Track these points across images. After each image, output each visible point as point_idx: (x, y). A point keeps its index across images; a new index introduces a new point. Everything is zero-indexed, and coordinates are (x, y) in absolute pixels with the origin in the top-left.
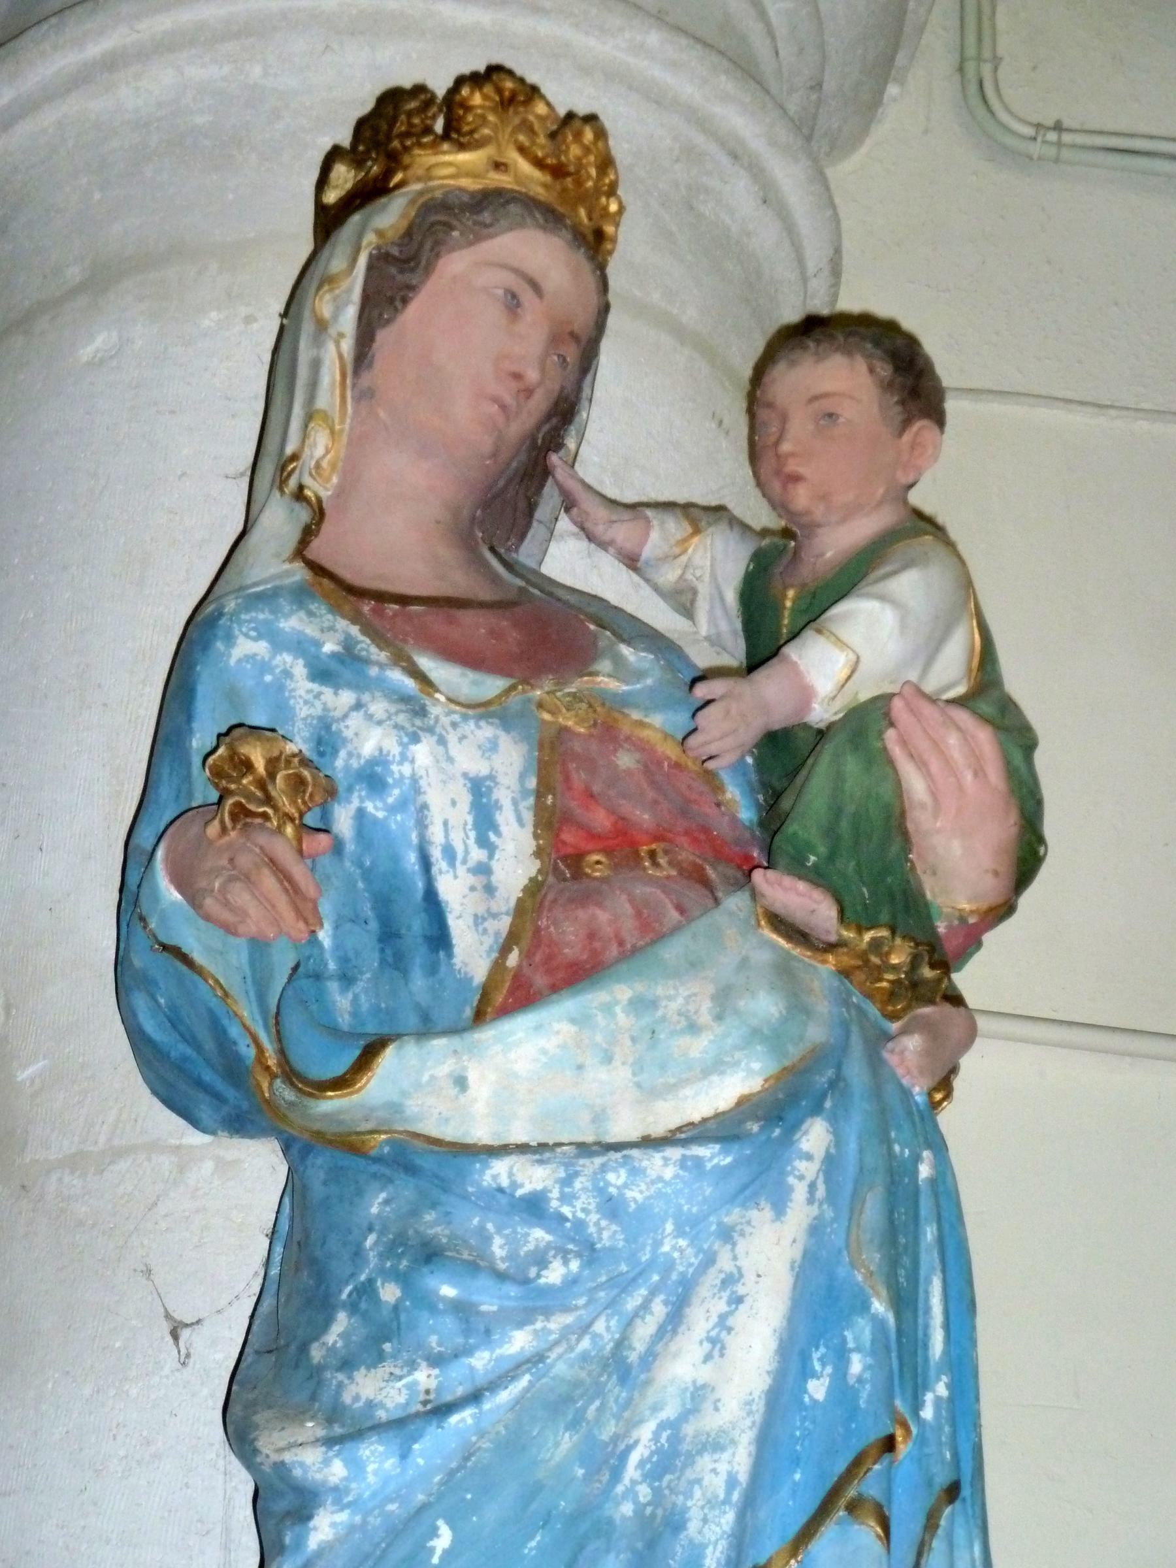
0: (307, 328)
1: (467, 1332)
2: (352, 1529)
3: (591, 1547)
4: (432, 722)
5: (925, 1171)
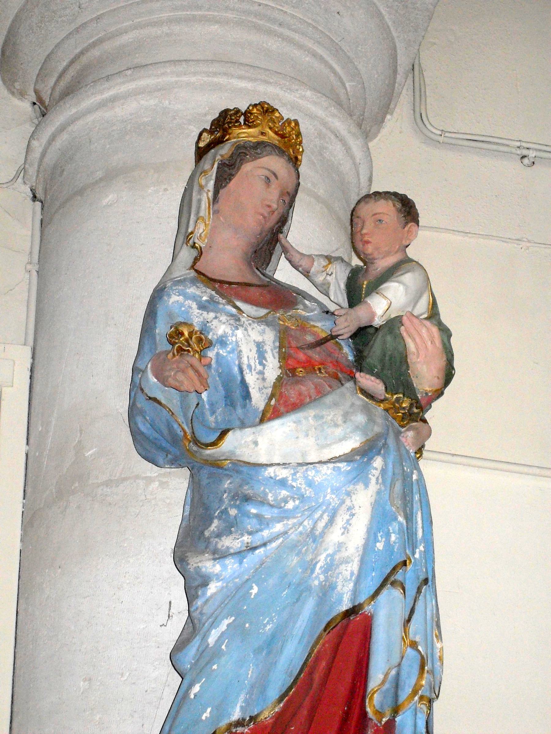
0: (196, 188)
1: (260, 524)
2: (222, 588)
3: (304, 594)
4: (242, 323)
5: (415, 477)
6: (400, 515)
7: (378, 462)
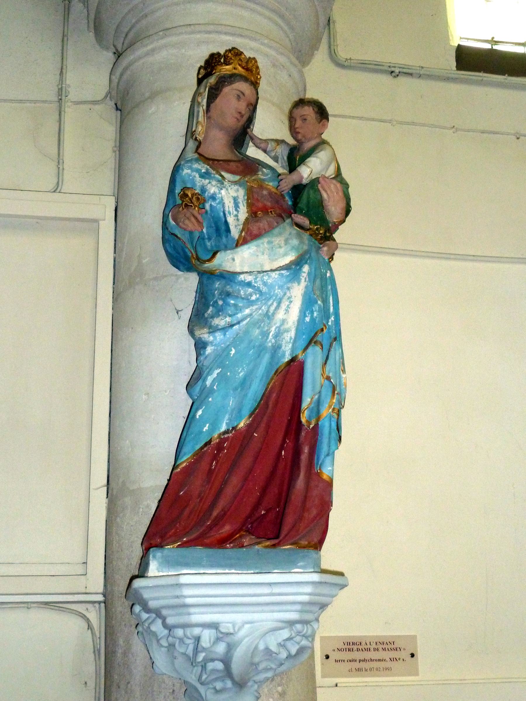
0: (196, 104)
1: (237, 310)
2: (214, 350)
5: (328, 275)
6: (319, 300)
7: (306, 268)
